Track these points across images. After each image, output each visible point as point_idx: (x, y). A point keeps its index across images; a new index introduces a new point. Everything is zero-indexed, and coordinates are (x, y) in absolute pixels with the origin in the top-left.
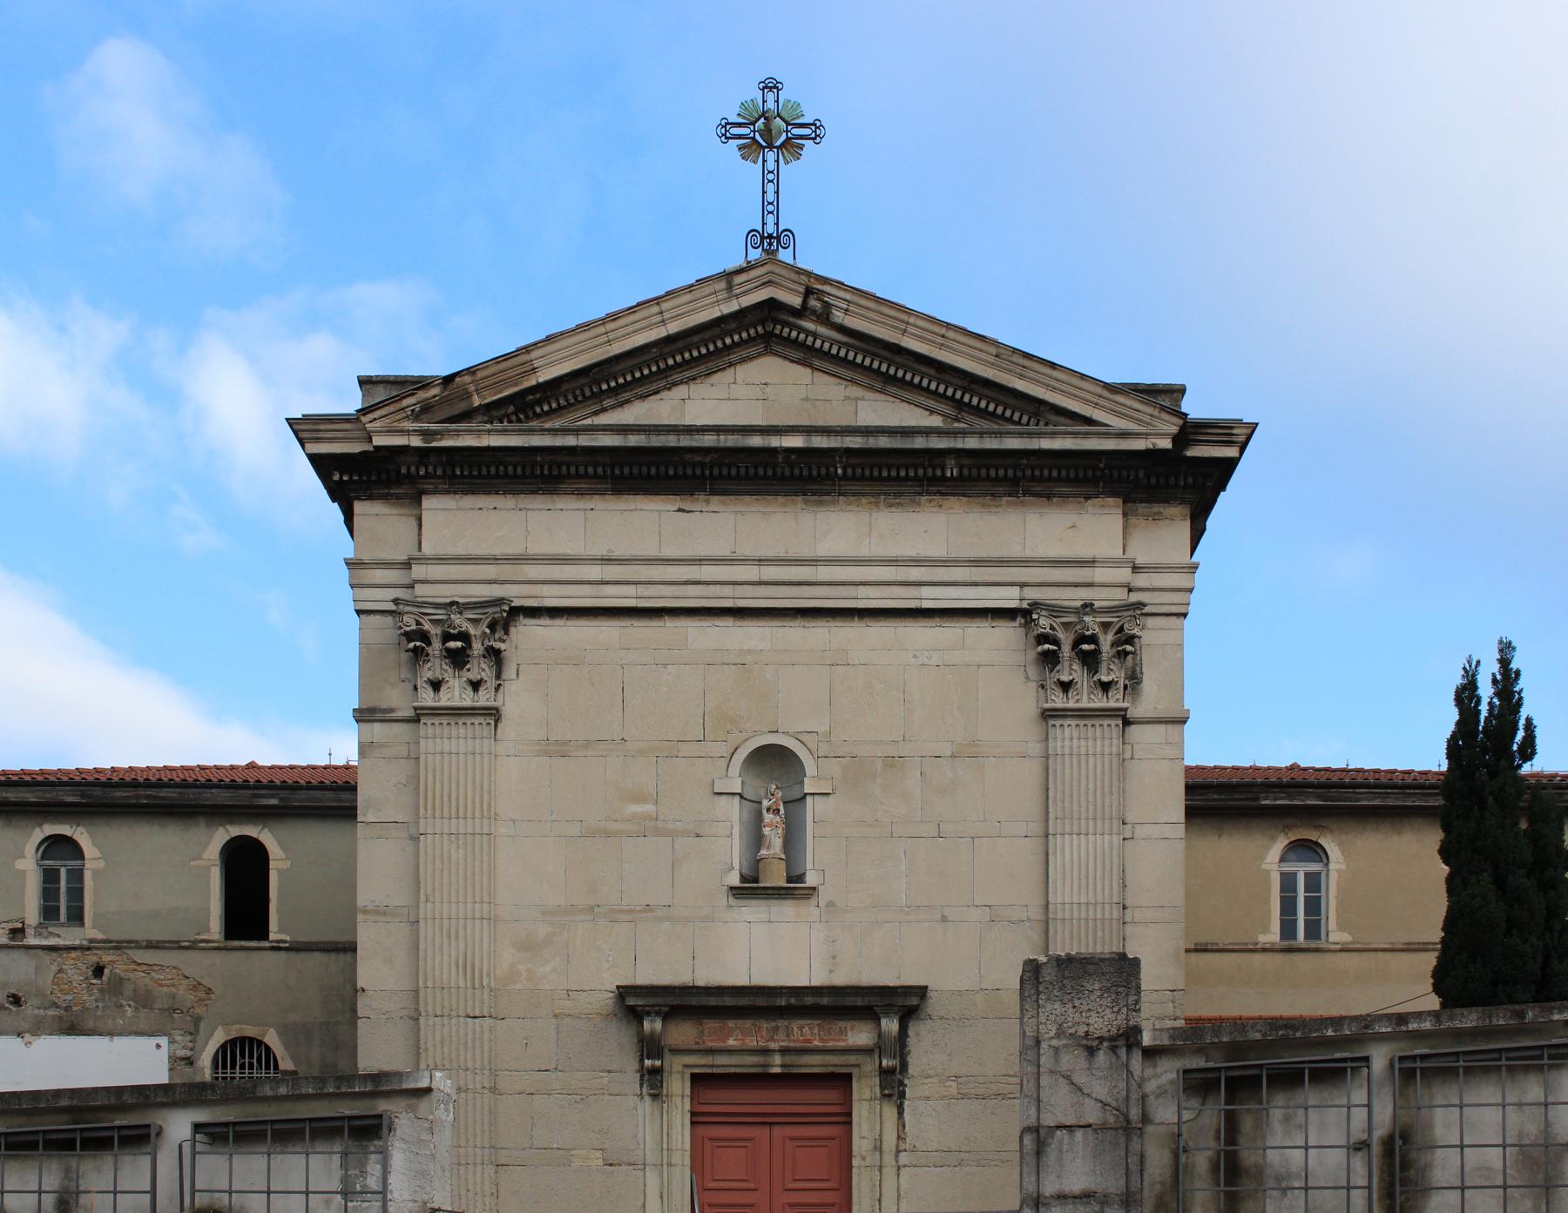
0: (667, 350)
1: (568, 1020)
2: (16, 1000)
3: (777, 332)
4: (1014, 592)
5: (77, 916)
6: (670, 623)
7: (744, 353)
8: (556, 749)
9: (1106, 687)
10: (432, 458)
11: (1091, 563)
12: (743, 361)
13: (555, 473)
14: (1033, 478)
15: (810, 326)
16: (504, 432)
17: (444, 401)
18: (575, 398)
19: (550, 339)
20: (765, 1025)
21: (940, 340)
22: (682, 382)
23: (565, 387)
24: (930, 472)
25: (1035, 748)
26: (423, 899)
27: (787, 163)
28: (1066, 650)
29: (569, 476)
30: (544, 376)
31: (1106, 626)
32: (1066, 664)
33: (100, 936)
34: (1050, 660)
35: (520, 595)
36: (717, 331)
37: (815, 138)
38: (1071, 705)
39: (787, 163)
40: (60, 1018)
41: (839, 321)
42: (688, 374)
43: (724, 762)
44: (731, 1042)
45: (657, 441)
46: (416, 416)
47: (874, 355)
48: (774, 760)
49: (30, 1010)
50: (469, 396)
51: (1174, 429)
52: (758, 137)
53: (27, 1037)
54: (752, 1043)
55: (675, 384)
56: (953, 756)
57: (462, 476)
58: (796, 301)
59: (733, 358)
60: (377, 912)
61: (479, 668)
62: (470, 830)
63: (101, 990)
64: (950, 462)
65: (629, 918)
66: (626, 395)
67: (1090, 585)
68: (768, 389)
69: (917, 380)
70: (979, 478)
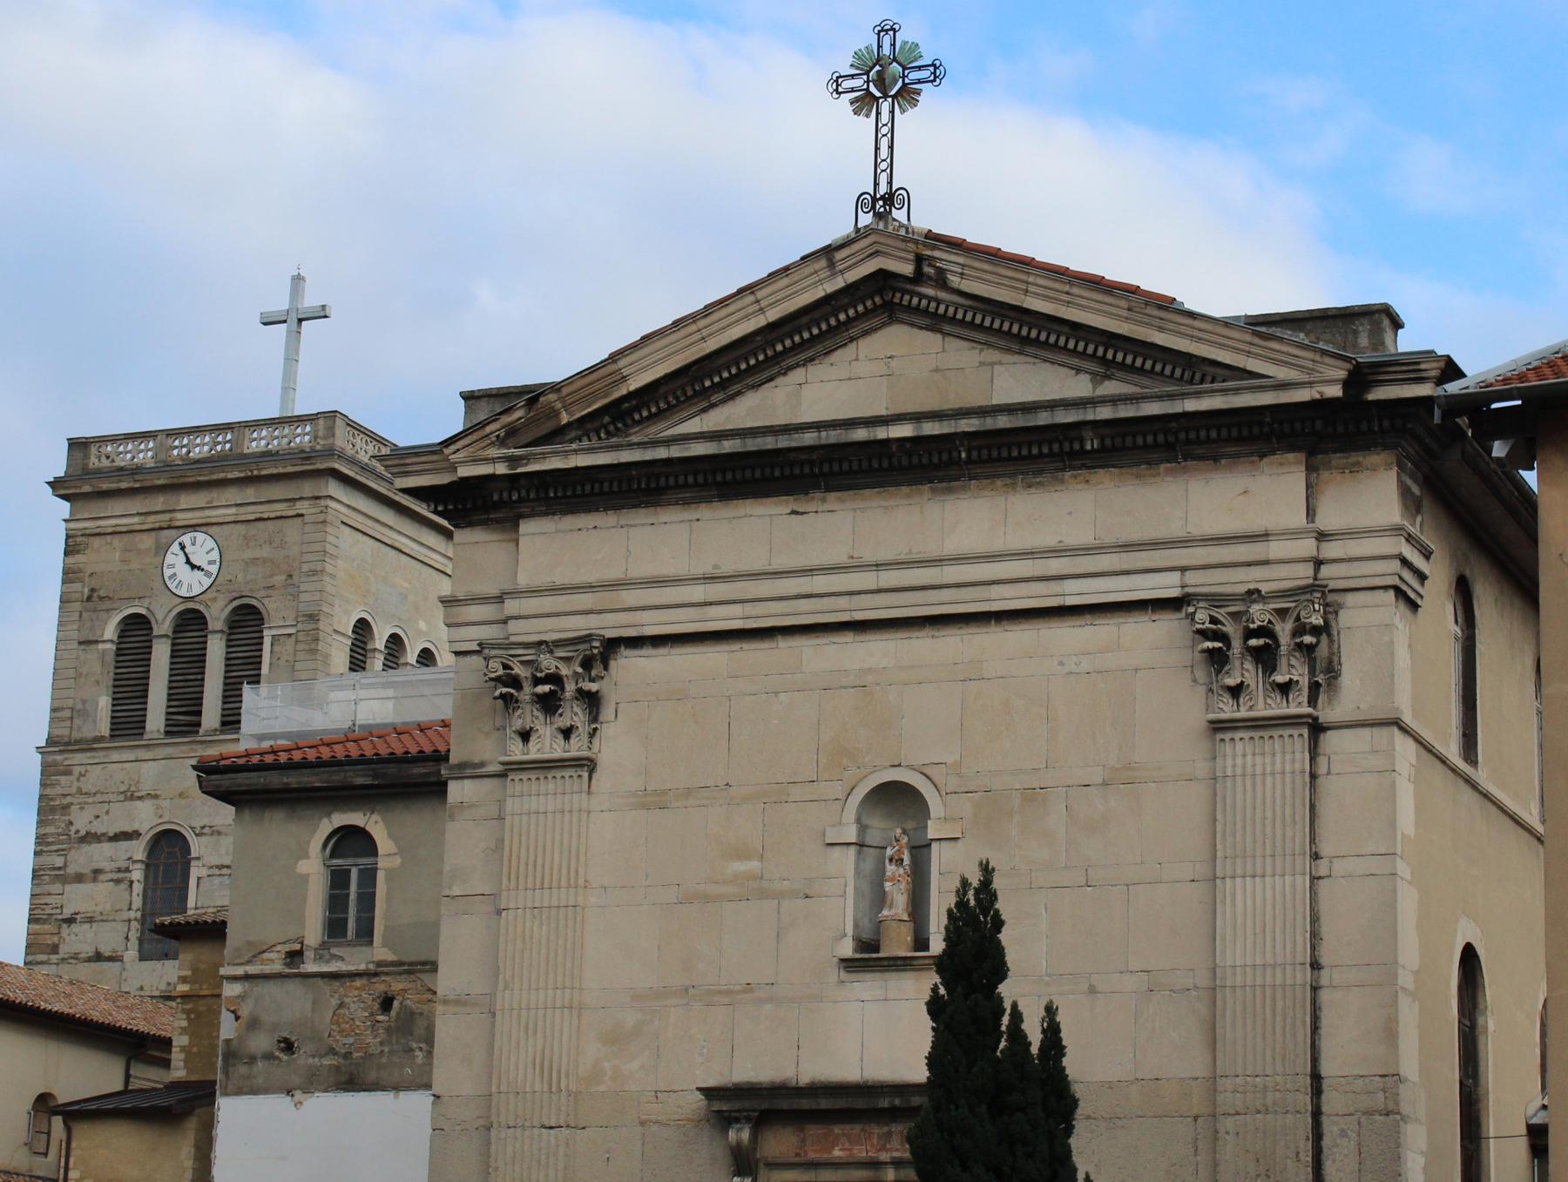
0: (774, 335)
1: (654, 1128)
2: (288, 1046)
3: (896, 300)
4: (1174, 578)
5: (366, 933)
6: (783, 643)
7: (865, 326)
8: (653, 800)
9: (1285, 689)
10: (523, 482)
11: (1265, 536)
12: (866, 333)
13: (653, 485)
14: (1188, 442)
15: (930, 291)
16: (591, 450)
17: (529, 423)
18: (677, 398)
19: (646, 339)
20: (876, 1130)
21: (1067, 298)
22: (798, 365)
23: (662, 390)
24: (1066, 445)
25: (1201, 768)
26: (501, 987)
27: (903, 111)
28: (1237, 644)
29: (668, 487)
30: (634, 384)
31: (1282, 613)
32: (1237, 663)
33: (390, 957)
34: (1218, 660)
35: (611, 625)
36: (828, 309)
37: (935, 78)
38: (1243, 713)
39: (903, 111)
40: (338, 1068)
41: (955, 286)
42: (803, 356)
43: (838, 805)
44: (837, 1153)
45: (753, 445)
46: (501, 442)
47: (1003, 318)
48: (895, 797)
49: (304, 1058)
50: (557, 414)
51: (1342, 374)
52: (873, 89)
53: (298, 1095)
54: (861, 1153)
55: (791, 368)
56: (1105, 784)
57: (556, 497)
58: (907, 269)
59: (853, 332)
60: (458, 1002)
61: (573, 714)
62: (572, 903)
63: (388, 1030)
64: (1087, 433)
65: (727, 1000)
66: (736, 388)
67: (1266, 563)
68: (894, 363)
69: (1052, 339)
70: (1124, 448)
